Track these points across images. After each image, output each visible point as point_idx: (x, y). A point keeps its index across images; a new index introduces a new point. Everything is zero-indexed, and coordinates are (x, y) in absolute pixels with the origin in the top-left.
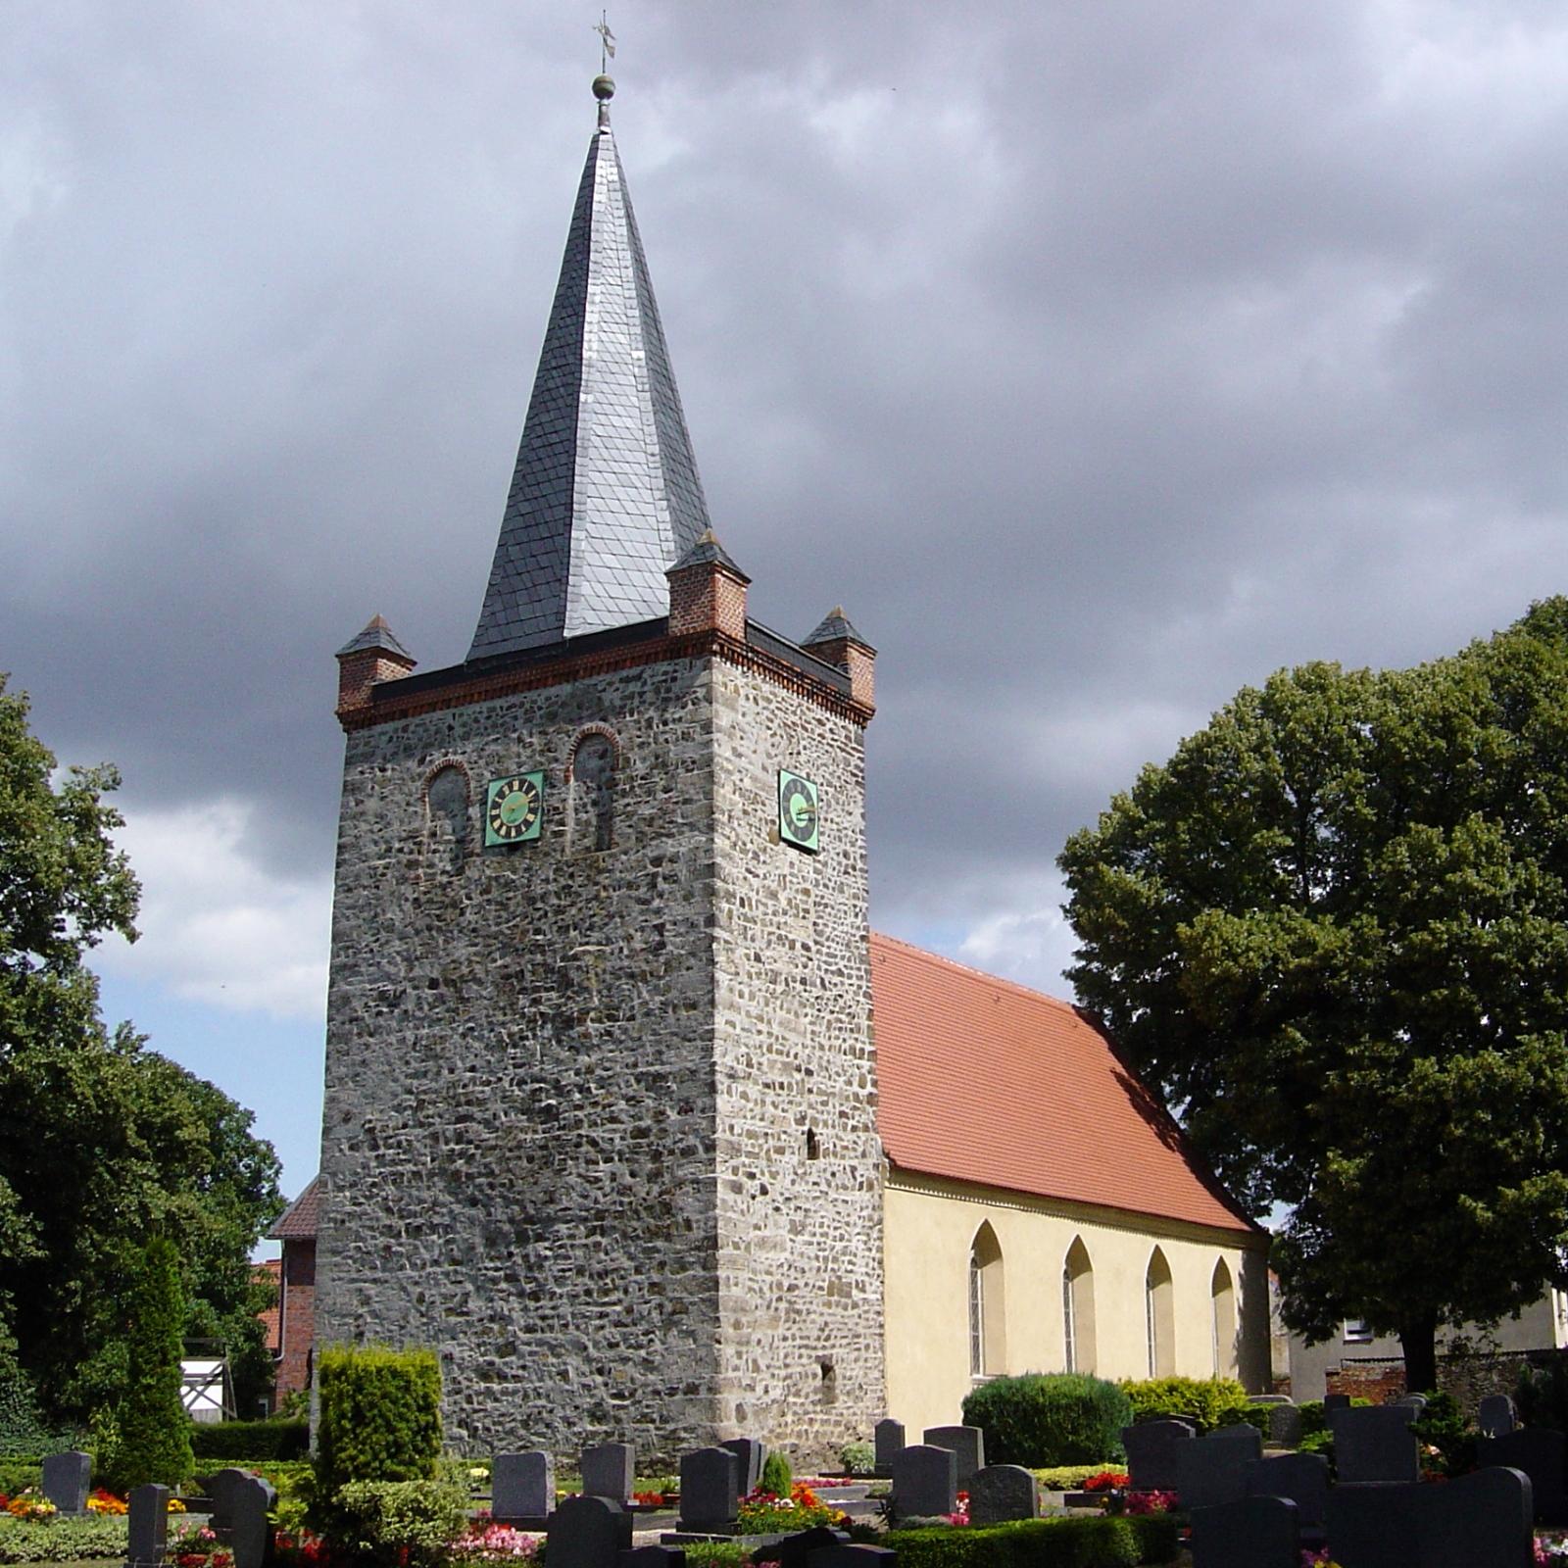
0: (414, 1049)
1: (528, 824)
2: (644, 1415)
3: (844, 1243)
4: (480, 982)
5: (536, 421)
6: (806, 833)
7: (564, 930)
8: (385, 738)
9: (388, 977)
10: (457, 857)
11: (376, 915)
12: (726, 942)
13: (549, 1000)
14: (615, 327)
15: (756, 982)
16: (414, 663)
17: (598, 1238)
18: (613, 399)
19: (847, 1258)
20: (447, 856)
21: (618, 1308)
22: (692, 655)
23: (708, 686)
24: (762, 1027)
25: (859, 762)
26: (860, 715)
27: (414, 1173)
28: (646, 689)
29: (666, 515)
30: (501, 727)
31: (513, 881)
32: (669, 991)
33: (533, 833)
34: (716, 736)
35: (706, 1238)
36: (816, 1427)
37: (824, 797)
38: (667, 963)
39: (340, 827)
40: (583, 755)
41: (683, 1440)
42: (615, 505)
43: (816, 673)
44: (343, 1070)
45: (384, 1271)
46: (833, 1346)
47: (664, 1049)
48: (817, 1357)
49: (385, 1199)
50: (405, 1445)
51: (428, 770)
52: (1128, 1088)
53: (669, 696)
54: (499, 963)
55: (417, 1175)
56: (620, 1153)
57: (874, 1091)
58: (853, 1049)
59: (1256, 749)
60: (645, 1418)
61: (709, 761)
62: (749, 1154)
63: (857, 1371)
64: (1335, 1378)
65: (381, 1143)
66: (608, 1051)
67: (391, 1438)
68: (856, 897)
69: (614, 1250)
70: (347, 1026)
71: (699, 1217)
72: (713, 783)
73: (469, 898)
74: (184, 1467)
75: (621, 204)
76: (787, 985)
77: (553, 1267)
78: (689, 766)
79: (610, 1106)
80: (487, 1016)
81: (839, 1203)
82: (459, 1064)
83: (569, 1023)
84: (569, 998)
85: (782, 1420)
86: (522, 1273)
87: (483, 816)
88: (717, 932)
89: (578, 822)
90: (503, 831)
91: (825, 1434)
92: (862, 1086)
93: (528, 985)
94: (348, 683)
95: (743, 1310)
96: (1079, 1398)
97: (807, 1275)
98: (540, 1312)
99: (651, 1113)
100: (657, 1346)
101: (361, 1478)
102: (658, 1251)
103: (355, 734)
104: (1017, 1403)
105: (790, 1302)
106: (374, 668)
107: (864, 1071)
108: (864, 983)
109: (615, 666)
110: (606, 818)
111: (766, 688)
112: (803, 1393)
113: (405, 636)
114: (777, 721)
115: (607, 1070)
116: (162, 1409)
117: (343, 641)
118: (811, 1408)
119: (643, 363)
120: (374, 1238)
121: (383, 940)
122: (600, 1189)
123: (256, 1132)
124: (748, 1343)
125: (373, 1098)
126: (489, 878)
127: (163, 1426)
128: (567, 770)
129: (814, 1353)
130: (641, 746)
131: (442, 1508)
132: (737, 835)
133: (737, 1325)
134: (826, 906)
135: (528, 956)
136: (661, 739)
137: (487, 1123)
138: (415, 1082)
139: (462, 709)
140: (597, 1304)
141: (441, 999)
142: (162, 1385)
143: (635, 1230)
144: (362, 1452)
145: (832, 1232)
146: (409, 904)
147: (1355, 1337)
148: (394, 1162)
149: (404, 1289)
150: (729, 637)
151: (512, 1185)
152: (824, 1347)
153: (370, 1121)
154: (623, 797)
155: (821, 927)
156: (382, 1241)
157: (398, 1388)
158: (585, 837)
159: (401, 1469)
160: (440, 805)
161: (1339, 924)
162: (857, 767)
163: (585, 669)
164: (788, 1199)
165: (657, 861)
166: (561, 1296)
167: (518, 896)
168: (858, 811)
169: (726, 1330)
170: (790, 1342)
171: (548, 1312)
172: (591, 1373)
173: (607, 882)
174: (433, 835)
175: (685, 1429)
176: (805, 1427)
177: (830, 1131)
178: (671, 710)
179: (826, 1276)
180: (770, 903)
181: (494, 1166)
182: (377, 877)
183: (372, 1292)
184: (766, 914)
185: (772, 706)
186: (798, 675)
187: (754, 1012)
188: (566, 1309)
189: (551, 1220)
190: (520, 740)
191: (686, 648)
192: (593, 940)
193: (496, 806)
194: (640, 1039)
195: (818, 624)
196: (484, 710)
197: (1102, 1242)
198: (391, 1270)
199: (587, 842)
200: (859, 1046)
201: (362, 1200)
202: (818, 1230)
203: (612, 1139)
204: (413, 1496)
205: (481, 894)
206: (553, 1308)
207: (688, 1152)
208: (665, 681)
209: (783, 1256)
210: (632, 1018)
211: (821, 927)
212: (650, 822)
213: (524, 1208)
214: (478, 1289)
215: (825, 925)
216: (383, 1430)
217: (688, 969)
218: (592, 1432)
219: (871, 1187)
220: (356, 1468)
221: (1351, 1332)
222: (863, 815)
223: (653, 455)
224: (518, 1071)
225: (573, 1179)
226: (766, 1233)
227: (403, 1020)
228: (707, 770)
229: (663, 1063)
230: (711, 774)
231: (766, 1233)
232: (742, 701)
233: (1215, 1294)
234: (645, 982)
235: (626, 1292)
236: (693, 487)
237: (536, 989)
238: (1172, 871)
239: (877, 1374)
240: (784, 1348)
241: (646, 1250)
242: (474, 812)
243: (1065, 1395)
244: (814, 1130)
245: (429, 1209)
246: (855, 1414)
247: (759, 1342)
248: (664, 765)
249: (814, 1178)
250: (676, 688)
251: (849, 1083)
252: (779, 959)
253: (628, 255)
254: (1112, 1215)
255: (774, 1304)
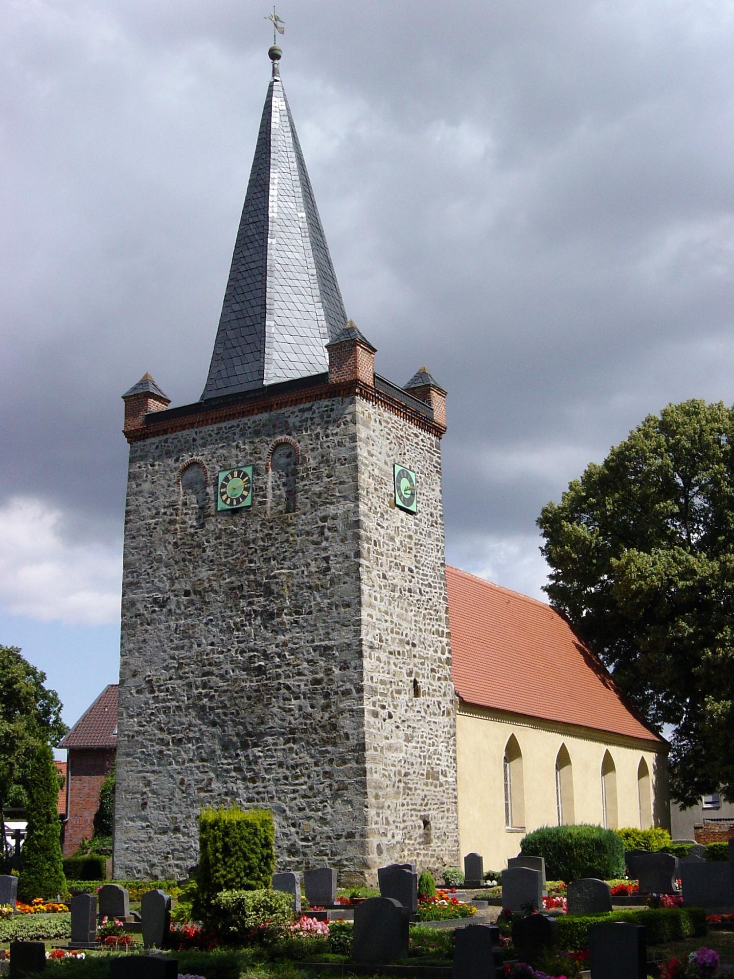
0: (176, 632)
1: (244, 497)
2: (321, 851)
3: (435, 748)
4: (216, 592)
5: (241, 255)
6: (410, 502)
7: (267, 560)
8: (154, 447)
9: (159, 590)
10: (200, 517)
11: (151, 552)
12: (367, 567)
13: (259, 602)
14: (287, 198)
15: (383, 591)
16: (169, 402)
17: (292, 745)
18: (288, 242)
19: (436, 757)
20: (194, 517)
21: (304, 787)
22: (343, 395)
23: (353, 414)
24: (388, 618)
25: (438, 459)
26: (438, 431)
27: (177, 707)
28: (314, 416)
29: (322, 312)
30: (226, 439)
31: (235, 531)
32: (333, 597)
33: (247, 502)
34: (358, 443)
35: (357, 745)
36: (421, 858)
37: (419, 480)
38: (332, 580)
39: (127, 500)
40: (277, 456)
41: (345, 866)
42: (291, 306)
43: (413, 406)
44: (132, 645)
45: (159, 765)
46: (430, 809)
47: (330, 631)
48: (421, 816)
49: (159, 722)
50: (255, 867)
51: (181, 465)
52: (582, 652)
53: (329, 419)
54: (228, 580)
55: (179, 708)
56: (304, 694)
57: (450, 656)
58: (437, 631)
59: (654, 451)
60: (322, 853)
61: (355, 458)
62: (382, 694)
63: (442, 824)
64: (700, 831)
65: (156, 689)
66: (295, 632)
67: (246, 864)
68: (438, 540)
69: (301, 752)
70: (134, 619)
71: (354, 732)
72: (357, 471)
73: (208, 542)
74: (61, 884)
75: (288, 124)
76: (401, 593)
77: (264, 763)
78: (343, 461)
79: (298, 665)
80: (221, 612)
81: (432, 724)
82: (204, 641)
83: (271, 616)
84: (271, 601)
85: (402, 854)
86: (245, 766)
87: (216, 493)
88: (362, 561)
89: (274, 496)
90: (228, 502)
91: (425, 862)
92: (443, 654)
93: (245, 594)
94: (130, 413)
95: (380, 788)
96: (593, 840)
97: (415, 766)
98: (256, 789)
99: (323, 670)
100: (329, 809)
101: (229, 888)
102: (329, 752)
103: (135, 444)
104: (555, 843)
105: (405, 783)
106: (147, 404)
107: (444, 644)
108: (443, 592)
109: (296, 402)
110: (292, 494)
111: (386, 415)
112: (413, 838)
113: (164, 385)
114: (392, 435)
115: (295, 644)
116: (48, 849)
117: (126, 387)
118: (417, 847)
119: (305, 220)
120: (152, 746)
121: (155, 568)
122: (292, 715)
123: (47, 685)
124: (383, 807)
125: (150, 662)
126: (220, 529)
127: (48, 860)
128: (267, 465)
129: (419, 814)
130: (313, 450)
131: (280, 906)
132: (372, 503)
133: (377, 797)
134: (421, 545)
135: (245, 577)
136: (325, 445)
137: (222, 677)
138: (177, 652)
139: (201, 429)
140: (291, 785)
141: (192, 603)
142: (47, 835)
143: (314, 740)
144: (229, 872)
145: (428, 741)
146: (170, 546)
147: (709, 806)
148: (164, 701)
149: (172, 777)
150: (365, 384)
151: (238, 713)
152: (425, 810)
153: (149, 676)
154: (302, 480)
155: (419, 558)
156: (157, 748)
157: (250, 834)
158: (278, 504)
159: (253, 882)
160: (189, 486)
161: (710, 558)
162: (437, 462)
163: (277, 404)
164: (404, 721)
165: (324, 519)
166: (269, 780)
167: (238, 541)
168: (438, 489)
169: (371, 800)
170: (406, 807)
171: (261, 790)
172: (288, 826)
173: (293, 531)
174: (185, 504)
175: (347, 860)
176: (415, 858)
177: (426, 680)
178: (331, 428)
179: (425, 767)
180: (391, 543)
181: (226, 702)
182: (150, 530)
183: (152, 779)
184: (388, 550)
185: (389, 426)
186: (404, 407)
187: (383, 609)
188: (272, 788)
189: (262, 735)
190: (237, 447)
191: (340, 391)
192: (285, 566)
193: (223, 486)
194: (315, 625)
195: (412, 376)
196: (215, 429)
197: (577, 747)
198: (162, 765)
199: (280, 508)
200: (441, 629)
201: (145, 723)
202: (420, 740)
203: (299, 686)
204: (263, 899)
205: (216, 539)
206: (264, 787)
207: (346, 693)
208: (327, 411)
209: (401, 755)
210: (310, 613)
211: (419, 558)
212: (319, 495)
213: (245, 728)
214: (217, 776)
215: (421, 557)
216: (242, 859)
217: (344, 583)
218: (289, 861)
219: (449, 714)
220: (226, 882)
221: (707, 803)
222: (441, 491)
223: (312, 275)
224: (240, 645)
225: (275, 710)
226: (391, 741)
227: (169, 615)
228: (354, 464)
229: (330, 640)
230: (356, 467)
231: (391, 741)
232: (372, 422)
233: (639, 779)
234: (318, 591)
235: (309, 777)
236: (336, 294)
237: (251, 596)
238: (606, 526)
239: (454, 827)
240: (402, 810)
241: (321, 752)
242: (210, 490)
243: (585, 838)
244: (417, 679)
245: (187, 728)
246: (442, 850)
247: (389, 806)
248: (328, 461)
249: (416, 709)
250: (333, 415)
251: (436, 651)
252: (396, 577)
253: (293, 154)
254: (582, 731)
255: (397, 784)
